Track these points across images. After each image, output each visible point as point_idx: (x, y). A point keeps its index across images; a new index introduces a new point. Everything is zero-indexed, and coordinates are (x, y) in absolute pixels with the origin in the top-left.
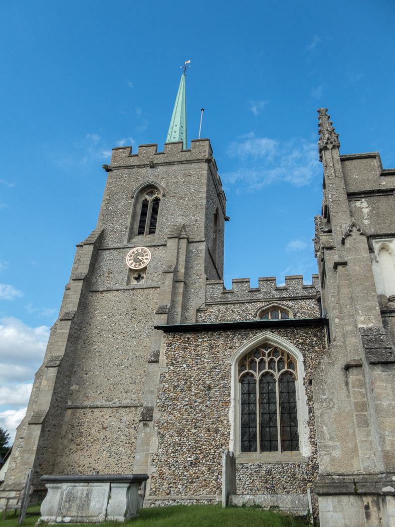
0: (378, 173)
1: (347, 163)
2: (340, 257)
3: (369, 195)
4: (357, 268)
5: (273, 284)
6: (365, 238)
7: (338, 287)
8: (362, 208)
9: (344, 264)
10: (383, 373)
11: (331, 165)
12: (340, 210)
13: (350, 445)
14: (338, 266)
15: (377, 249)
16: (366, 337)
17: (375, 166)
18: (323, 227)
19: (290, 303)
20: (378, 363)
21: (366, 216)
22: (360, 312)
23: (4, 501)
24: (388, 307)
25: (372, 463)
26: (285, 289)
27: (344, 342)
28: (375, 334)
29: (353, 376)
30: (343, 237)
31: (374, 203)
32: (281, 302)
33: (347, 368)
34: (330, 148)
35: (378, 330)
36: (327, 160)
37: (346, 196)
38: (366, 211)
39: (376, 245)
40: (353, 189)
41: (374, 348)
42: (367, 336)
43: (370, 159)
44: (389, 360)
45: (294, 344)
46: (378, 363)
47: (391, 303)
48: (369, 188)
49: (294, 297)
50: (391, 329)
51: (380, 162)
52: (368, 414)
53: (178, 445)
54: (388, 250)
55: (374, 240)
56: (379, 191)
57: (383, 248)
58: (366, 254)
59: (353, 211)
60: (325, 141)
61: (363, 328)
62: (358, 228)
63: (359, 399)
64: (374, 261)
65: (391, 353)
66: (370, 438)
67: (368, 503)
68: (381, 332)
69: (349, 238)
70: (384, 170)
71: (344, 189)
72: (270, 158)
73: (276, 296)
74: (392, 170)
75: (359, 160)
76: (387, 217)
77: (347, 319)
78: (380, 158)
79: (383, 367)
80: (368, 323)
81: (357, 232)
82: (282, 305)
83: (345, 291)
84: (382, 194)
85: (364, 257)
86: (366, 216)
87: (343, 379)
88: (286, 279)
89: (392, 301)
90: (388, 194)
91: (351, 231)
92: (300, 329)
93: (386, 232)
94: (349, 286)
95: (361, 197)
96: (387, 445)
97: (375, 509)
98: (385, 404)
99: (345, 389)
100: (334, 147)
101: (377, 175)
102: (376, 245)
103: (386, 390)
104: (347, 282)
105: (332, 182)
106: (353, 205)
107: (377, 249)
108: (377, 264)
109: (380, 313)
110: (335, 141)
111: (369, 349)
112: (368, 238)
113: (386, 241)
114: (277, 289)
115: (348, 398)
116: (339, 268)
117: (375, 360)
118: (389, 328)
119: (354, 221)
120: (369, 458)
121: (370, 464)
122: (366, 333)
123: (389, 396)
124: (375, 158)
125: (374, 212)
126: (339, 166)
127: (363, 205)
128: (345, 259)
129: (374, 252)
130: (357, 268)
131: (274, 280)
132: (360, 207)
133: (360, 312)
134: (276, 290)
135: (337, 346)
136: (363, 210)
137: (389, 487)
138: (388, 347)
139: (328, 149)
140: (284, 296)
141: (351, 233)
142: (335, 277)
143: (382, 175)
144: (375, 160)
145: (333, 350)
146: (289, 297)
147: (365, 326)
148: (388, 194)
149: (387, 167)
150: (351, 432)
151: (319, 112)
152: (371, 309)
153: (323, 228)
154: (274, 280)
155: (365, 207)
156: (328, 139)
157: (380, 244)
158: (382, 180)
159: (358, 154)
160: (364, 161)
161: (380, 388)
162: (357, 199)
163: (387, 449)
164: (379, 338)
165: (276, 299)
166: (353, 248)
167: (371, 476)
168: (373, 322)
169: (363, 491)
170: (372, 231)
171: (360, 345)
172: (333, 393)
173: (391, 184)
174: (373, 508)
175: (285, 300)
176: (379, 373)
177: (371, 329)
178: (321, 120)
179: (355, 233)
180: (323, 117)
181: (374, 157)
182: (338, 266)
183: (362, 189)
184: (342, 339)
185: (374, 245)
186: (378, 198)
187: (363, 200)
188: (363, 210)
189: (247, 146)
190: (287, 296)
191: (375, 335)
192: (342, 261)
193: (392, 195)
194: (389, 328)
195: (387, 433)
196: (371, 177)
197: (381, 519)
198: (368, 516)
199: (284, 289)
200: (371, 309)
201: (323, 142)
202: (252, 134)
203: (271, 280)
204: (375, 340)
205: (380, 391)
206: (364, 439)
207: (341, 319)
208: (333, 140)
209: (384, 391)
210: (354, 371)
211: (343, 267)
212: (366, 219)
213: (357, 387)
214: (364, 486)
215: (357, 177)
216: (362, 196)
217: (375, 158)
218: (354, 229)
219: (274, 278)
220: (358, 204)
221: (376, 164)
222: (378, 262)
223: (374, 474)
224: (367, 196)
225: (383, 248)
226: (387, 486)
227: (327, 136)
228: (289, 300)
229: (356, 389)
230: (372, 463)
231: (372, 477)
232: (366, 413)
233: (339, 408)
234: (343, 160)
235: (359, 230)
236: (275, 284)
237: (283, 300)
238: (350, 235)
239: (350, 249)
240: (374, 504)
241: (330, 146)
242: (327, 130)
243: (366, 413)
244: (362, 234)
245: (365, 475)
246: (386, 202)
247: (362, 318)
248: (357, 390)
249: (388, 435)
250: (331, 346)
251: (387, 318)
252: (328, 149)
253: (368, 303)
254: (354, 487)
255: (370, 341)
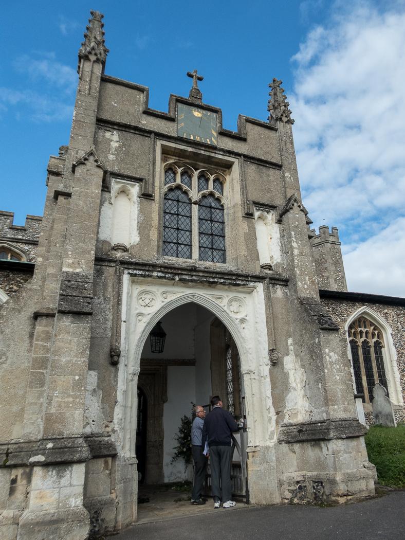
0: (141, 109)
1: (110, 86)
2: (65, 187)
3: (124, 129)
4: (81, 203)
5: (9, 221)
6: (101, 172)
7: (53, 222)
8: (111, 141)
9: (68, 195)
10: (72, 325)
11: (87, 80)
12: (83, 134)
13: (15, 409)
14: (59, 196)
15: (114, 190)
16: (67, 283)
17: (140, 101)
18: (63, 152)
19: (26, 247)
20: (69, 313)
21: (113, 151)
22: (70, 253)
23: (404, 379)
24: (109, 255)
25: (36, 429)
26: (23, 230)
27: (42, 287)
28: (79, 280)
29: (41, 327)
30: (74, 163)
31: (126, 139)
32: (14, 244)
33: (37, 316)
34: (92, 60)
35: (86, 277)
36: (85, 72)
37: (94, 120)
38: (114, 145)
39: (115, 185)
40: (106, 116)
41: (71, 296)
42: (69, 281)
43: (137, 91)
44: (84, 310)
45: (6, 291)
46: (69, 313)
47: (114, 252)
48: (126, 120)
49: (32, 241)
50: (105, 279)
51: (147, 98)
52: (47, 373)
53: (334, 383)
54: (128, 195)
55: (114, 179)
56: (136, 129)
57: (123, 191)
58: (97, 190)
59: (100, 140)
60: (88, 49)
61: (67, 273)
62: (96, 158)
63: (40, 354)
64: (107, 202)
65: (89, 303)
66: (41, 400)
67: (17, 476)
68: (87, 280)
69: (82, 167)
70: (149, 109)
71: (94, 111)
72: (68, 92)
73: (9, 236)
74: (157, 112)
75: (124, 88)
76: (136, 158)
77: (52, 259)
78: (148, 94)
79: (74, 318)
80: (75, 268)
81: (93, 162)
82: (14, 247)
83: (59, 226)
84: (138, 133)
85: (92, 193)
86: (113, 151)
87: (28, 329)
88: (27, 218)
89: (115, 250)
90: (145, 134)
91: (86, 159)
92: (18, 274)
93: (131, 175)
94: (66, 222)
95: (114, 129)
96: (52, 407)
97: (24, 482)
98: (64, 360)
99: (28, 342)
100: (97, 61)
101: (139, 111)
102: (115, 185)
103: (70, 344)
104: (65, 217)
105: (83, 98)
106: (101, 134)
107: (114, 190)
108: (111, 206)
109: (93, 258)
110: (101, 54)
111: (64, 295)
112: (105, 172)
113: (128, 184)
114: (12, 228)
115: (29, 353)
116: (61, 198)
117: (66, 308)
118: (103, 278)
119: (94, 149)
120: (33, 424)
121: (34, 430)
122: (69, 278)
123: (71, 351)
124: (143, 92)
125: (124, 149)
126: (96, 84)
127: (114, 138)
128: (71, 190)
129: (110, 192)
130: (81, 203)
131: (10, 216)
132: (109, 139)
133: (70, 253)
134: (11, 228)
135: (31, 290)
136: (112, 143)
137: (40, 456)
138: (88, 296)
139: (89, 60)
140: (20, 237)
141: (86, 162)
142: (53, 209)
143: (145, 112)
144: (142, 95)
145: (24, 294)
146: (27, 240)
147: (71, 270)
148: (145, 134)
149: (152, 107)
150: (21, 393)
151: (92, 13)
152: (85, 252)
153: (62, 154)
154: (10, 216)
155: (115, 140)
156: (93, 49)
157: (120, 186)
158: (143, 119)
159: (119, 78)
160: (130, 91)
161: (63, 341)
162: (108, 129)
163: (52, 412)
164: (83, 285)
165: (8, 240)
166: (84, 179)
167: (30, 444)
168: (82, 268)
169: (13, 463)
170: (116, 169)
171: (59, 291)
172: (9, 346)
173: (152, 126)
174: (21, 482)
175: (19, 242)
176: (67, 324)
177: (77, 274)
178: (91, 24)
179: (91, 163)
180: (96, 22)
181: (141, 90)
182: (59, 196)
183: (117, 119)
184: (40, 283)
185: (112, 184)
186: (132, 135)
187: (115, 132)
188: (112, 143)
189: (43, 66)
190: (24, 238)
191: (79, 282)
192: (67, 191)
193: (150, 137)
194: (103, 278)
195: (56, 393)
196: (132, 110)
197: (28, 493)
198: (12, 491)
199: (21, 230)
200: (85, 252)
201: (85, 50)
202: (52, 55)
203: (7, 215)
204: (77, 288)
205: (61, 344)
206: (33, 401)
207: (46, 259)
208: (98, 52)
209: (67, 345)
210: (43, 321)
211: (65, 199)
212: (112, 154)
213: (42, 340)
214: (16, 456)
215: (116, 105)
216: (115, 127)
217: (143, 92)
218: (91, 159)
219: (12, 214)
220: (108, 135)
221: (141, 99)
222: (111, 204)
223: (34, 442)
224: (120, 129)
225: (123, 192)
226: (38, 454)
227: (93, 44)
228: (26, 243)
229: (39, 343)
230: (36, 429)
231: (31, 445)
232: (44, 371)
233: (12, 364)
234: (104, 80)
235: (96, 161)
236: (12, 222)
237: (17, 242)
238: (84, 164)
239: (79, 179)
240: (24, 476)
241: (93, 58)
242: (95, 38)
243: (44, 371)
244: (98, 166)
245: (23, 443)
246: (140, 143)
247: (70, 261)
248: (41, 343)
249: (57, 396)
250: (23, 289)
251: (104, 268)
252: (89, 60)
253: (83, 245)
254: (5, 458)
255: (70, 285)
